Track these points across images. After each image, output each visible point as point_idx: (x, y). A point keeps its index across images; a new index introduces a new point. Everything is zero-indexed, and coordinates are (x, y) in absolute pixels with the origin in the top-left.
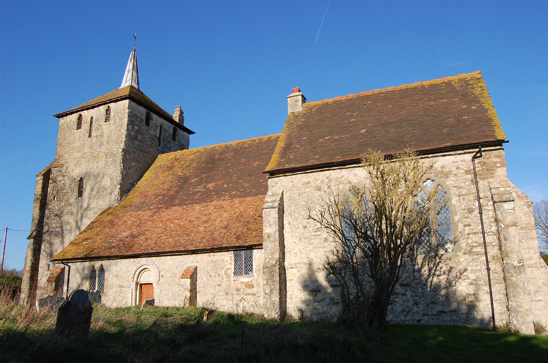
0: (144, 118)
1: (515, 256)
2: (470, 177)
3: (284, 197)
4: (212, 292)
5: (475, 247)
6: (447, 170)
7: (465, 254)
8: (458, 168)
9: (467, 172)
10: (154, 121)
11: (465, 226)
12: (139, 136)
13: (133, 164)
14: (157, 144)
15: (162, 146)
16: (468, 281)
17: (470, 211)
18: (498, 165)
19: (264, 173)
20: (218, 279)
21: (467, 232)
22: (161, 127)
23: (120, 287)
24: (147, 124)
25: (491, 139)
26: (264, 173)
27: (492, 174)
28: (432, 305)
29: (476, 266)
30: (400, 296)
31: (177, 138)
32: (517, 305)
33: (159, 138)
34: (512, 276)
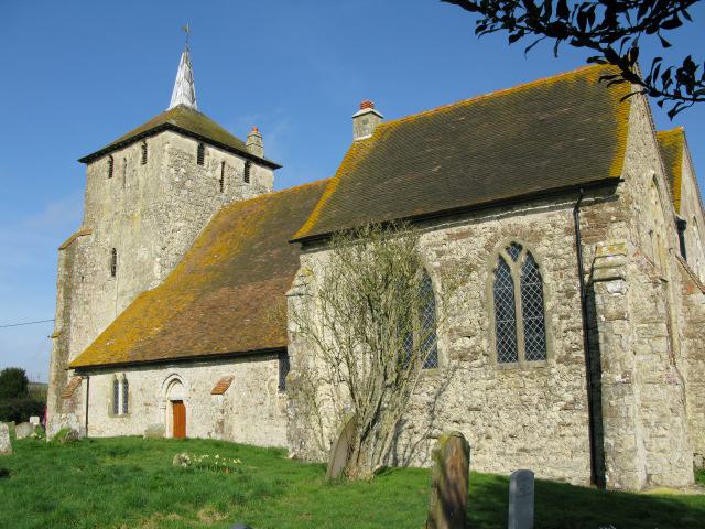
0: (195, 154)
1: (619, 366)
2: (570, 239)
3: (677, 235)
4: (252, 413)
5: (575, 350)
6: (538, 229)
7: (559, 362)
8: (554, 225)
9: (567, 231)
10: (212, 157)
11: (561, 318)
12: (189, 184)
13: (179, 224)
14: (218, 189)
15: (225, 191)
16: (562, 403)
17: (570, 294)
18: (614, 218)
19: (290, 242)
20: (259, 395)
21: (564, 327)
22: (223, 164)
23: (146, 405)
24: (200, 161)
25: (600, 177)
26: (290, 242)
27: (604, 233)
28: (510, 440)
29: (575, 381)
30: (468, 425)
31: (251, 177)
32: (616, 444)
33: (221, 181)
34: (611, 398)
